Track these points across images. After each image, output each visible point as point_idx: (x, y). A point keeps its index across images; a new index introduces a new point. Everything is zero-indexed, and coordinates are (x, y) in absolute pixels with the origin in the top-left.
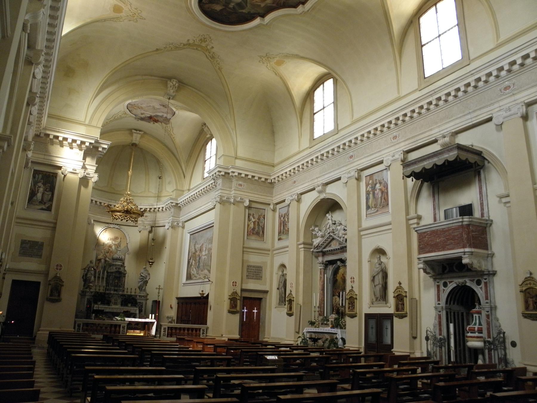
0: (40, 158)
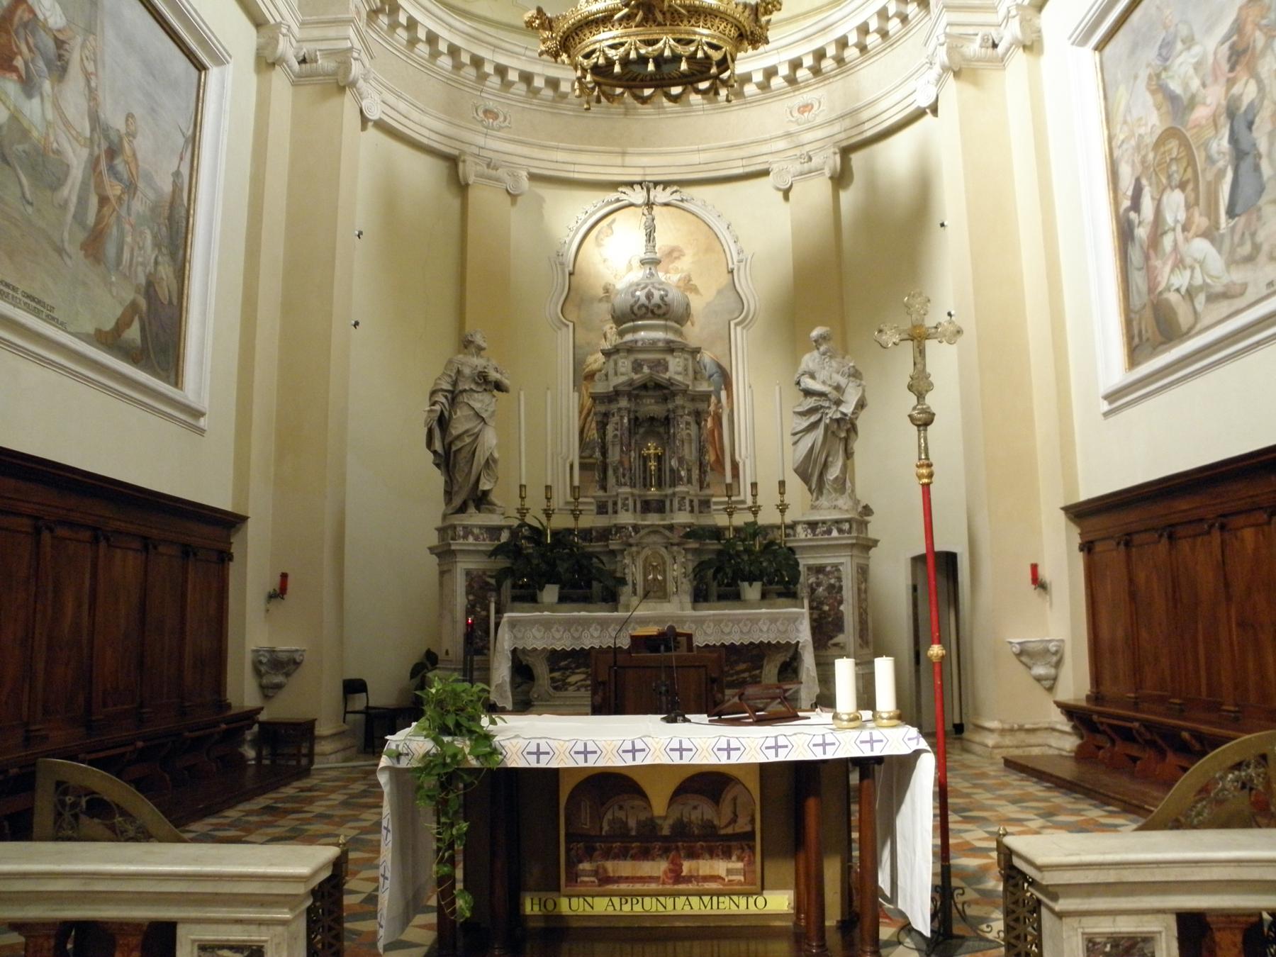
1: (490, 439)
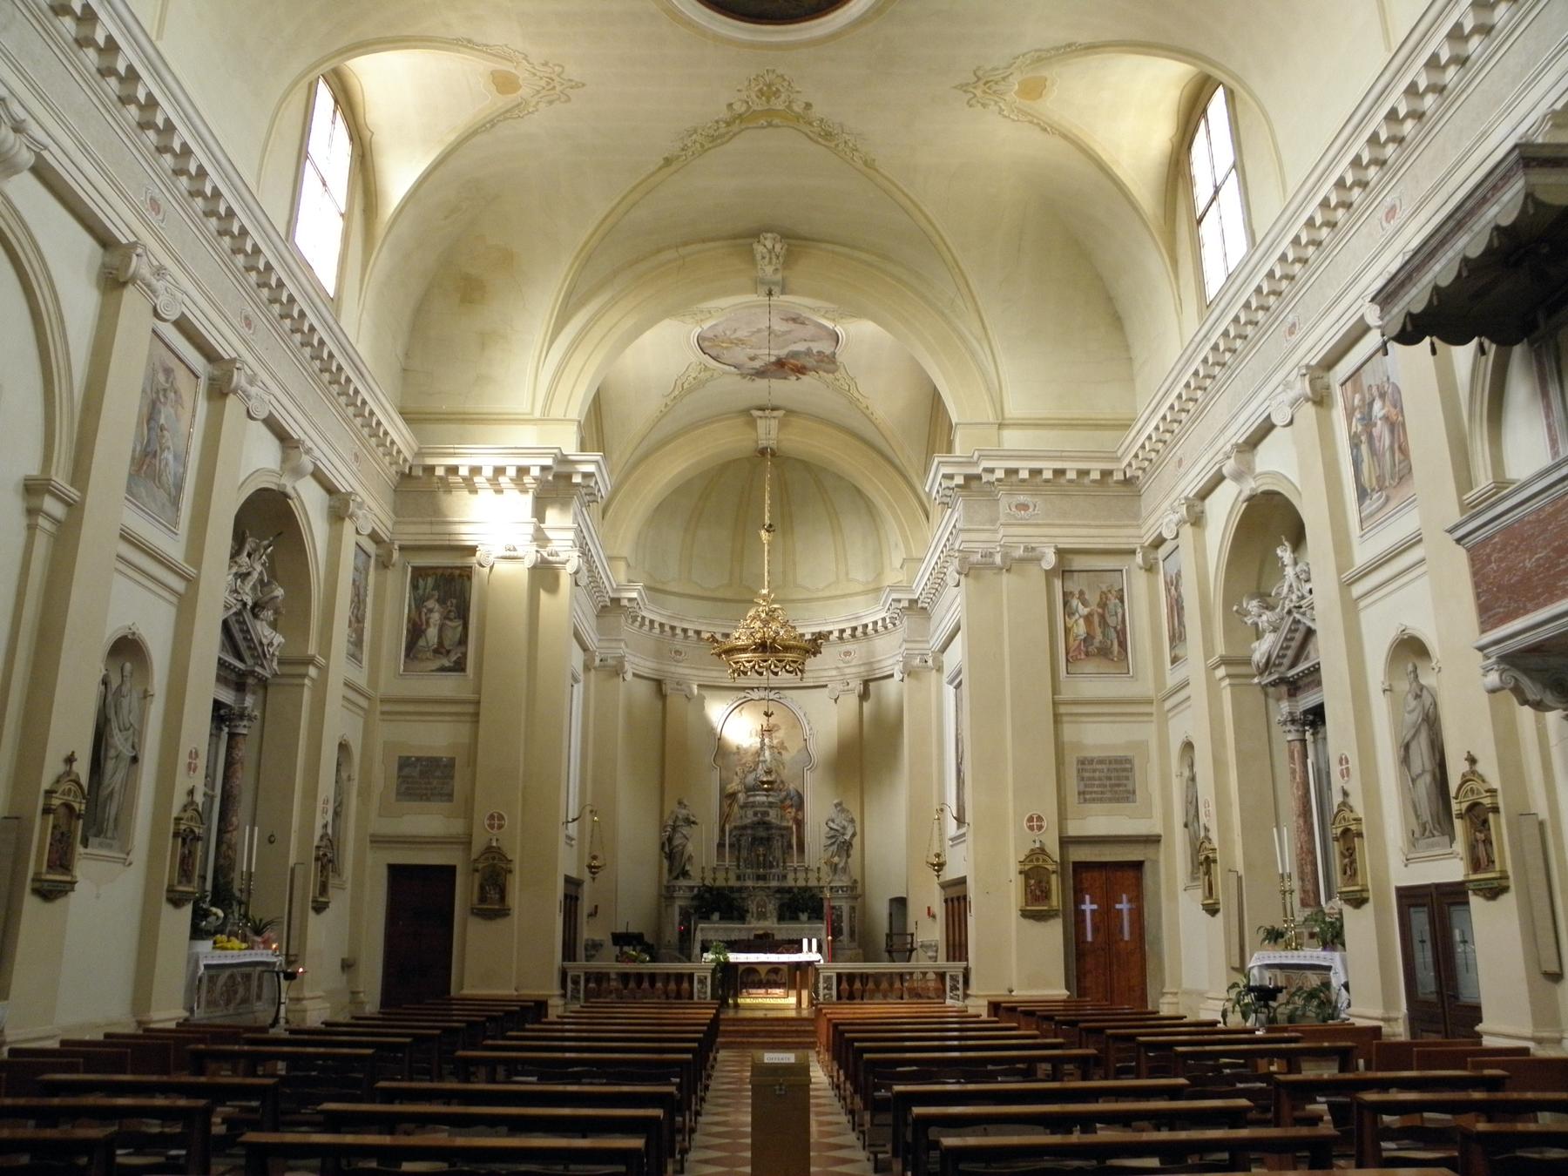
0: (415, 533)
1: (690, 848)
